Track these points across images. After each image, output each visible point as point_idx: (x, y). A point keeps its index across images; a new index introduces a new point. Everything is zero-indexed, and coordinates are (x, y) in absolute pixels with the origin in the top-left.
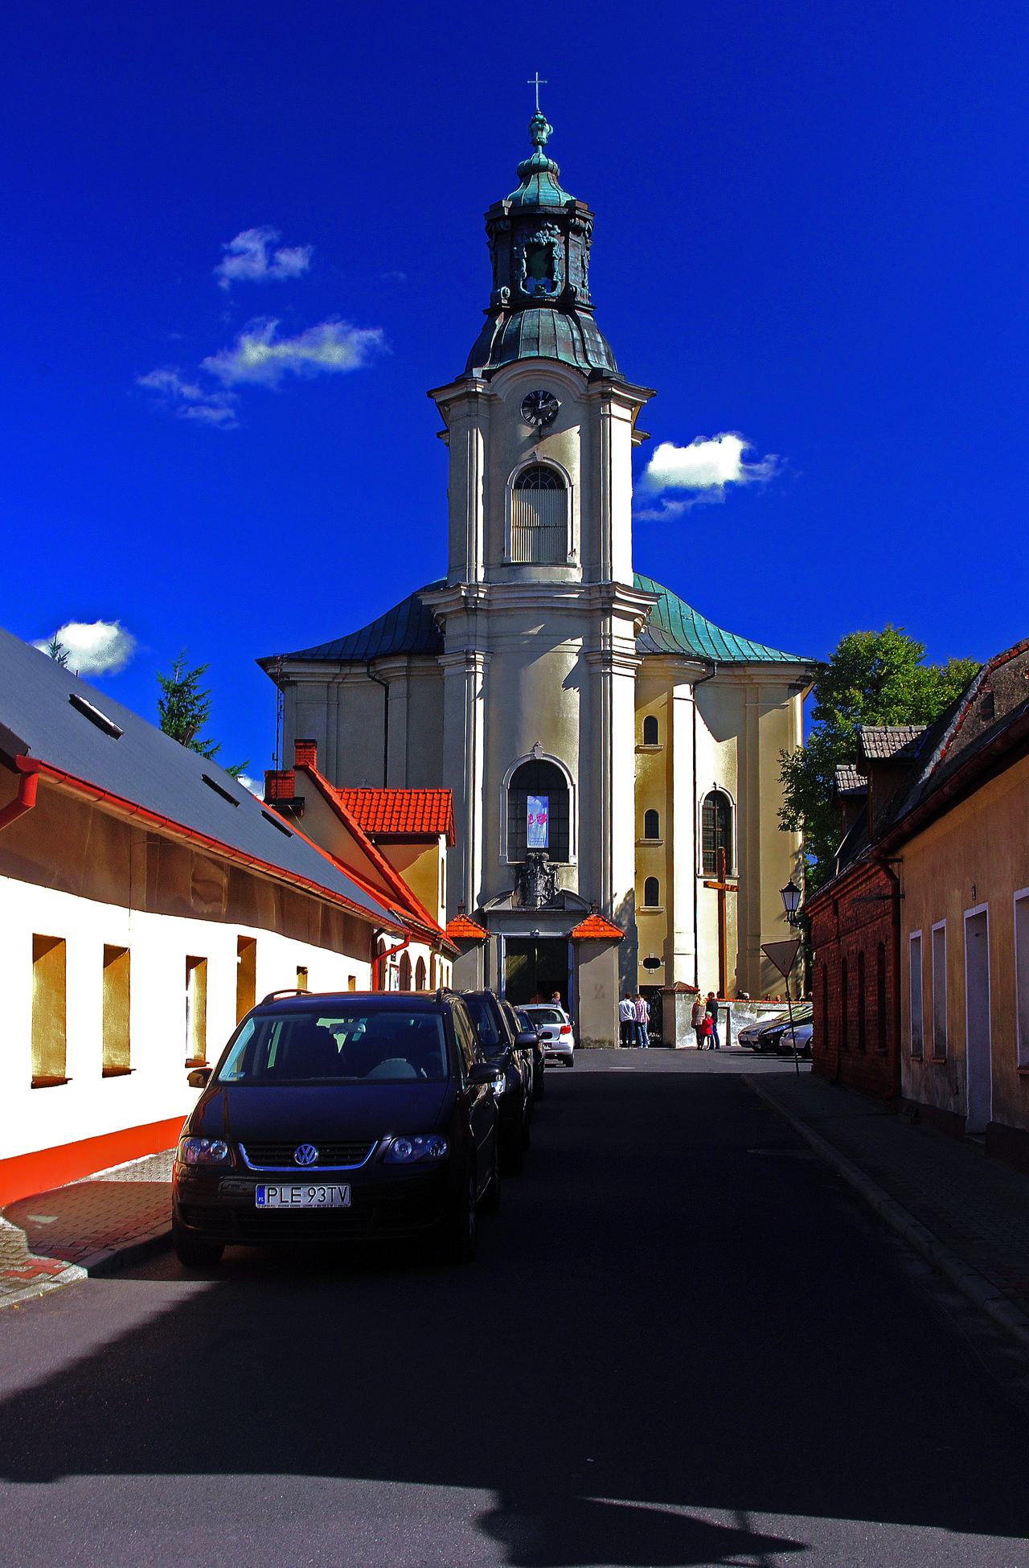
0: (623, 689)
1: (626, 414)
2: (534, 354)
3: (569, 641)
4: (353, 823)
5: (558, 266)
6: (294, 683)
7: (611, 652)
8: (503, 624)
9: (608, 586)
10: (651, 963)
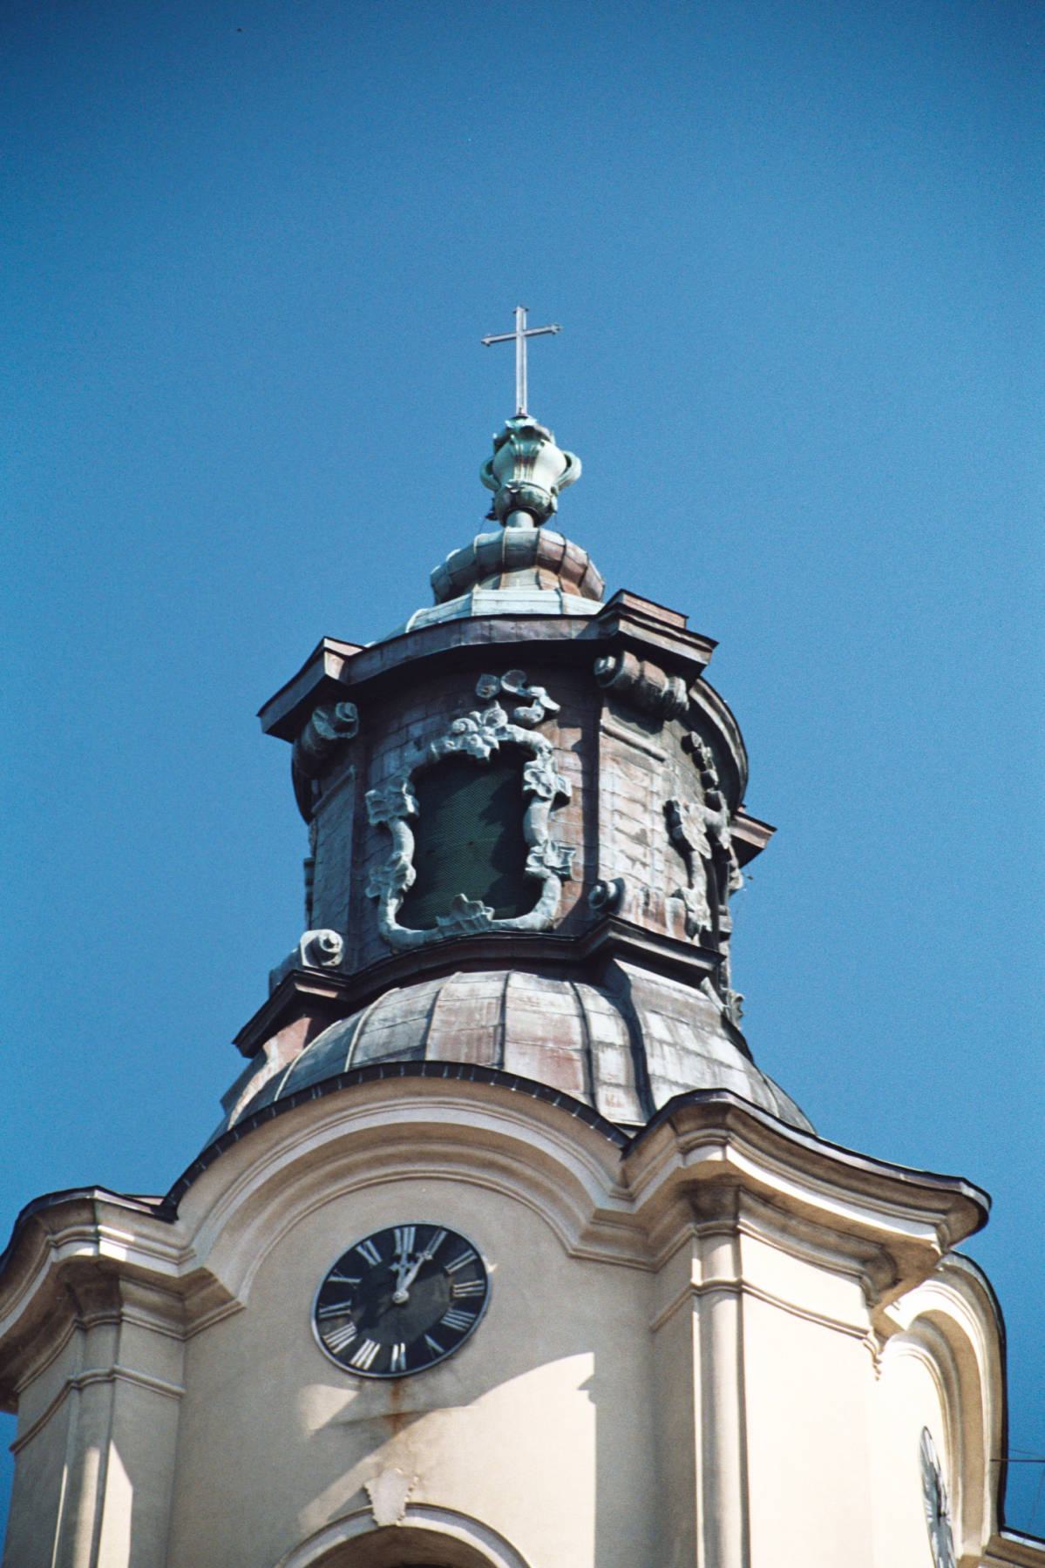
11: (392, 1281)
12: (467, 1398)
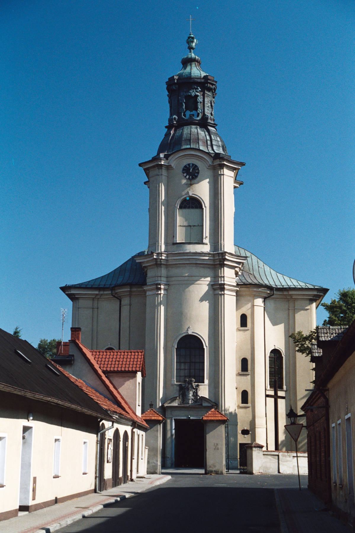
0: (229, 300)
1: (232, 174)
2: (188, 147)
3: (203, 279)
4: (97, 366)
5: (200, 106)
7: (224, 284)
8: (175, 271)
9: (222, 253)
10: (245, 432)
11: (190, 169)
12: (198, 183)
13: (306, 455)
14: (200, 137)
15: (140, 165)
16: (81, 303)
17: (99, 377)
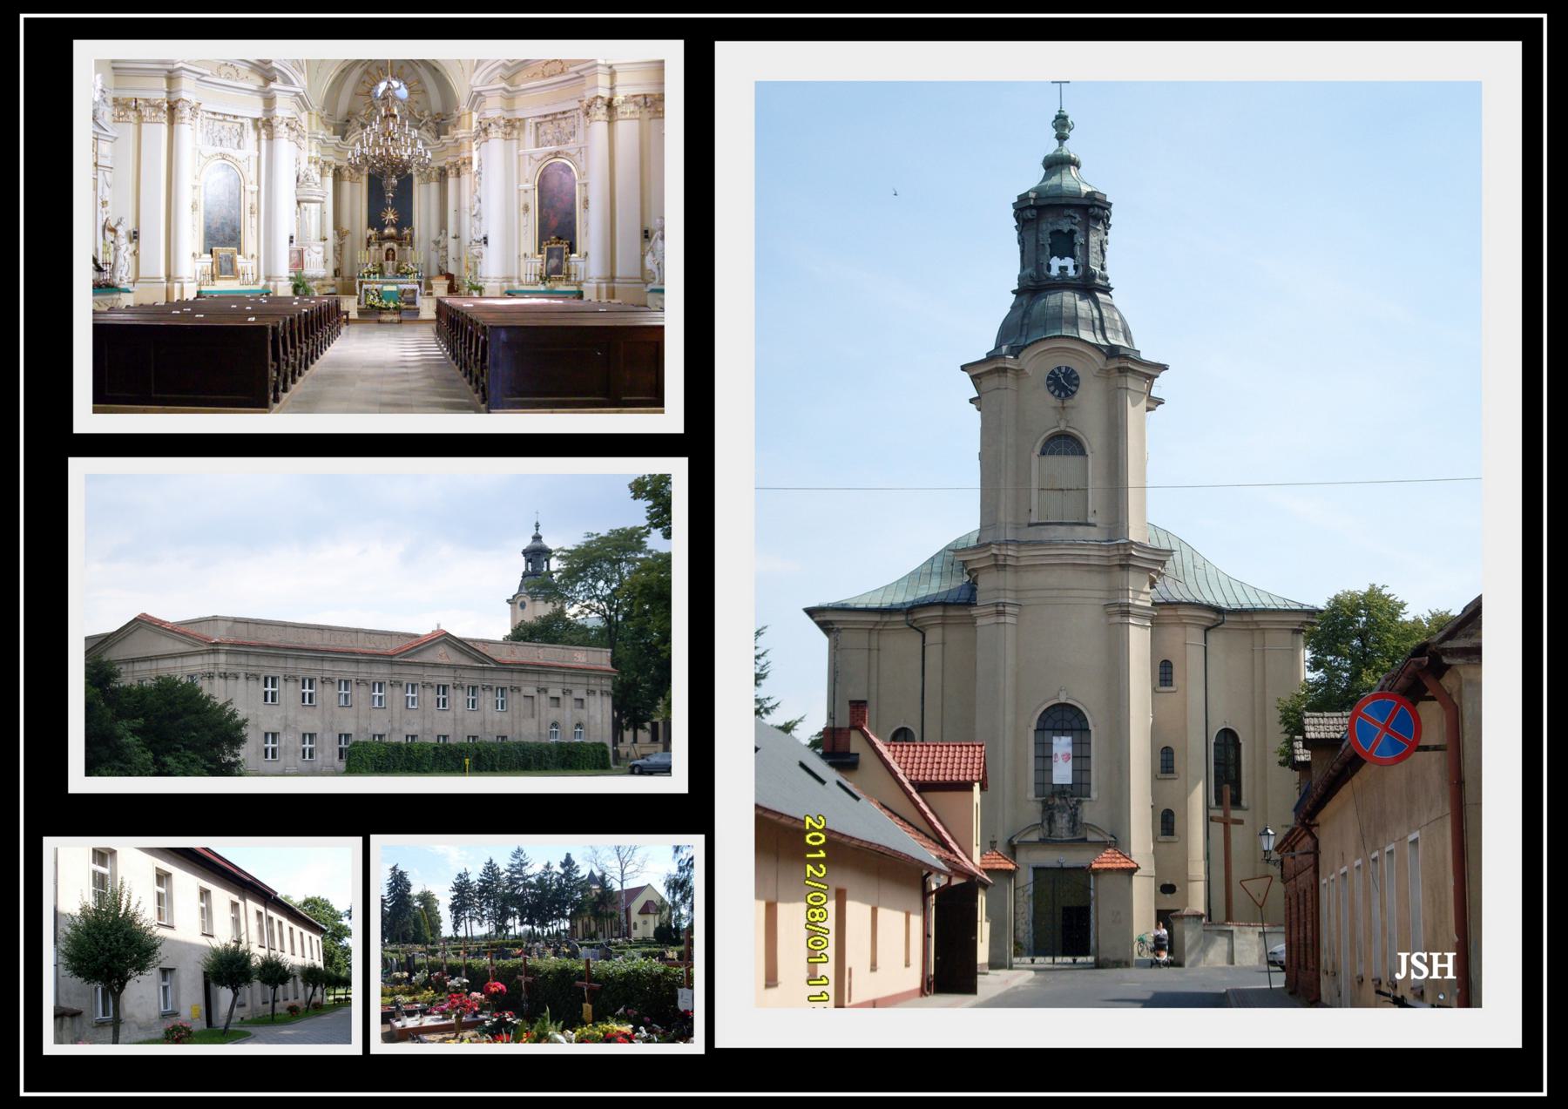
6: (839, 630)
13: (1283, 929)
14: (1081, 313)
15: (963, 368)
16: (845, 637)
17: (909, 794)
